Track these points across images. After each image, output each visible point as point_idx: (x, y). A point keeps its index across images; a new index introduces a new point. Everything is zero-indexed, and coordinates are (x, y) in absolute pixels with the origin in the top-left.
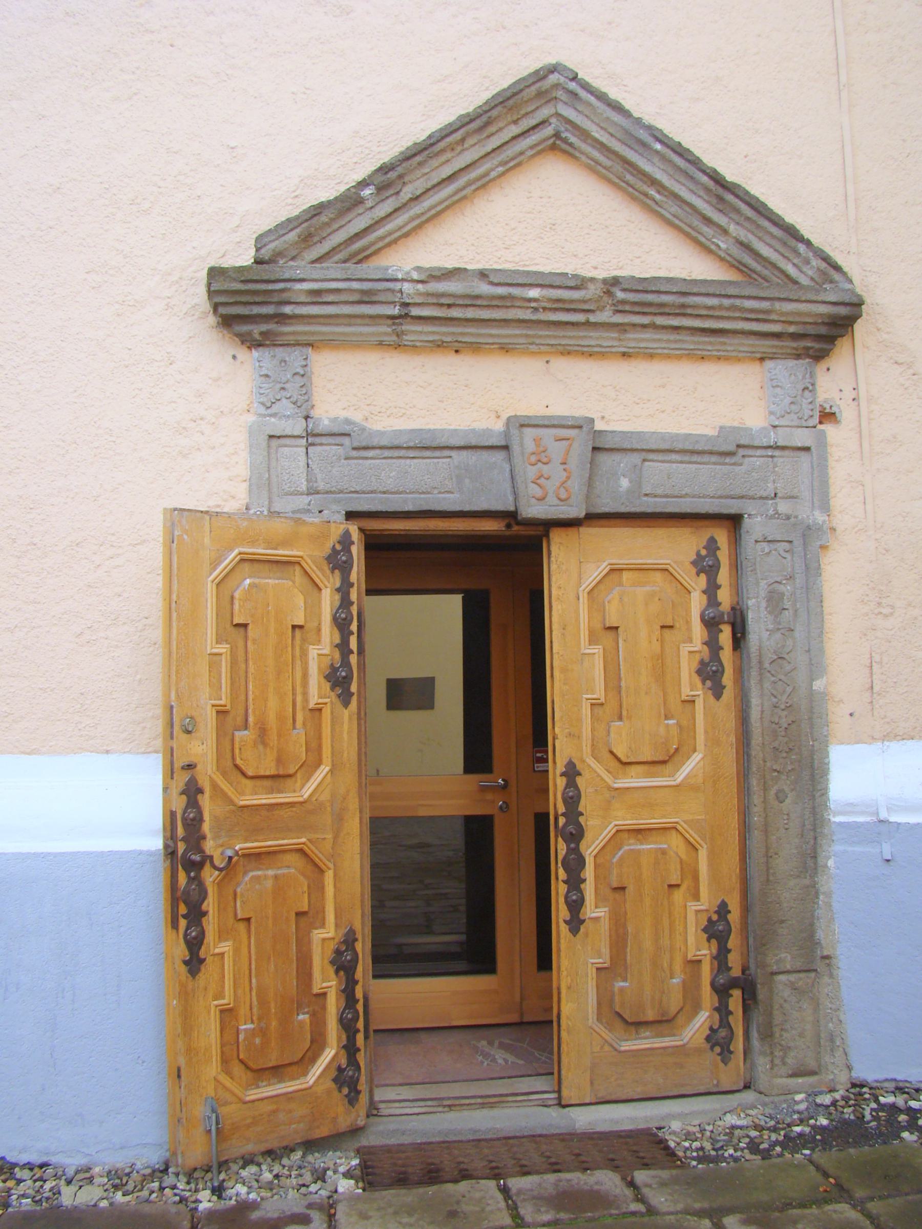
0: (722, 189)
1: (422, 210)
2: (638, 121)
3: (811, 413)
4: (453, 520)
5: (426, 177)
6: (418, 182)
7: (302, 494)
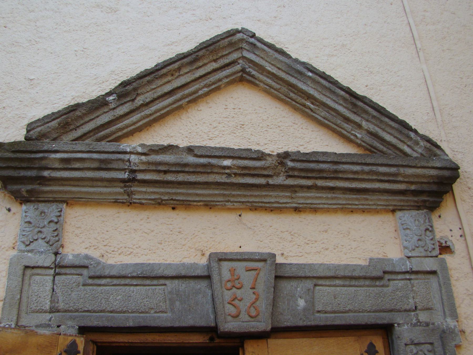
0: (354, 99)
1: (150, 112)
2: (296, 60)
3: (433, 247)
4: (167, 334)
5: (153, 91)
6: (148, 94)
7: (46, 312)
